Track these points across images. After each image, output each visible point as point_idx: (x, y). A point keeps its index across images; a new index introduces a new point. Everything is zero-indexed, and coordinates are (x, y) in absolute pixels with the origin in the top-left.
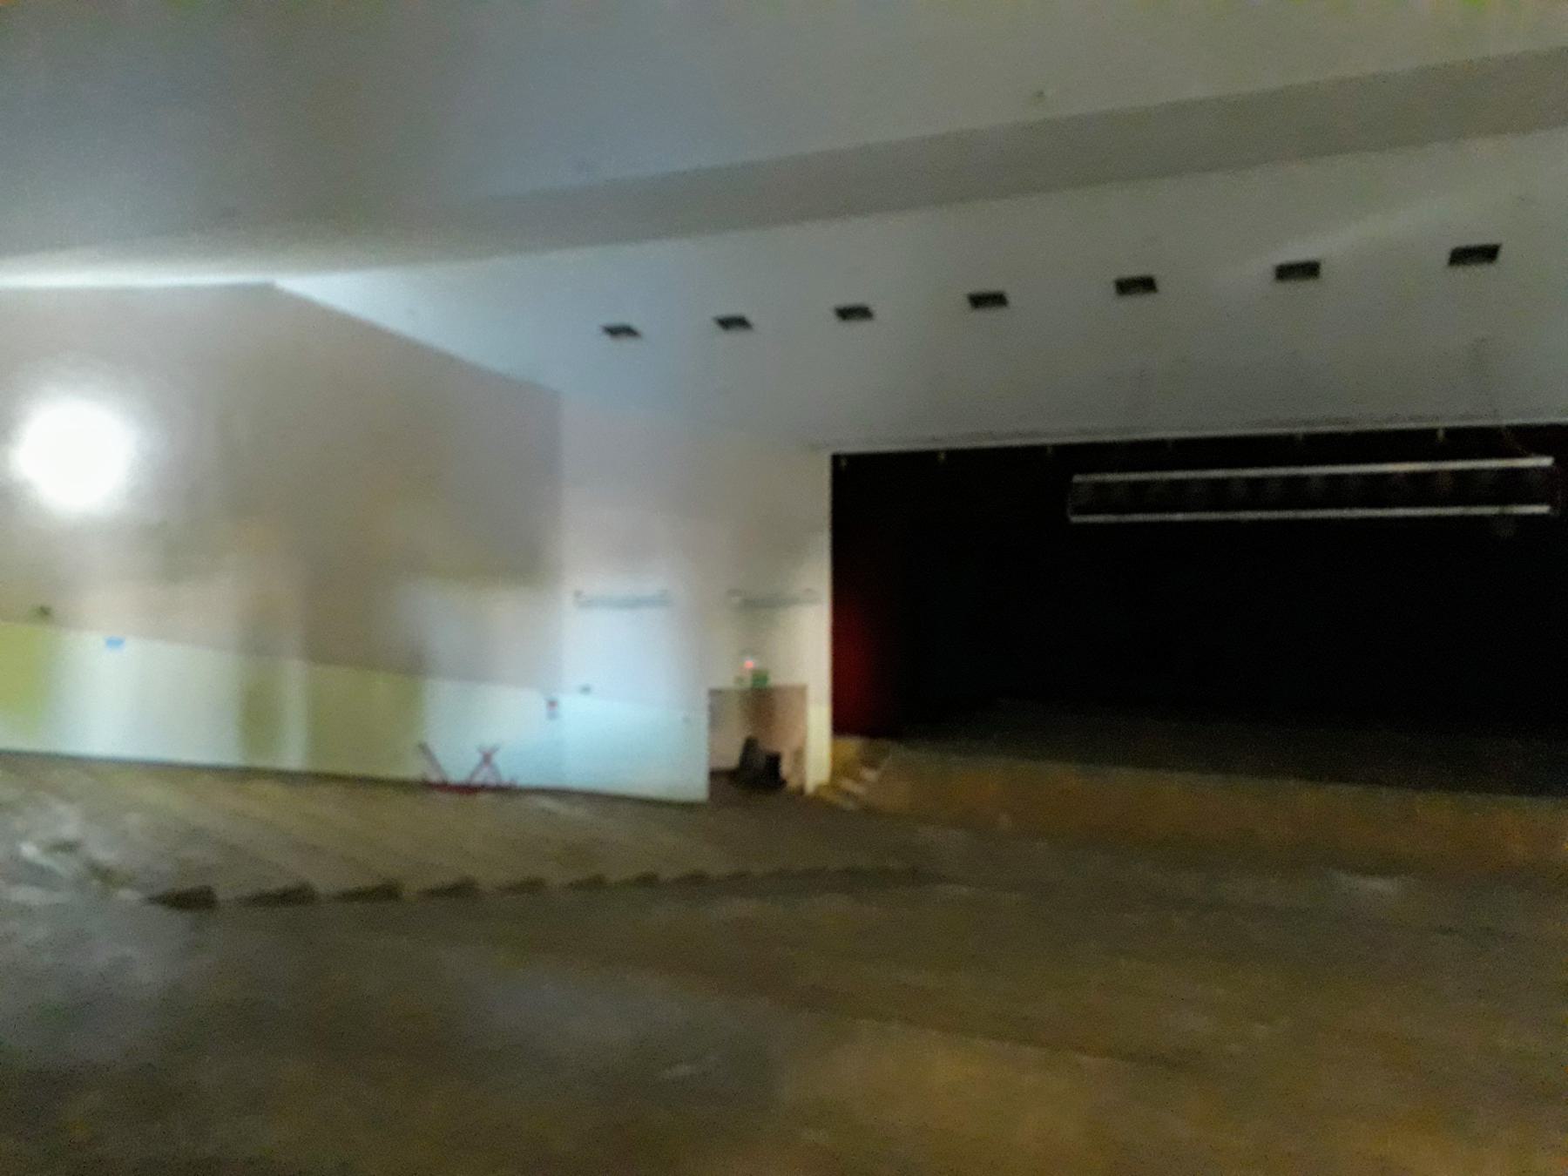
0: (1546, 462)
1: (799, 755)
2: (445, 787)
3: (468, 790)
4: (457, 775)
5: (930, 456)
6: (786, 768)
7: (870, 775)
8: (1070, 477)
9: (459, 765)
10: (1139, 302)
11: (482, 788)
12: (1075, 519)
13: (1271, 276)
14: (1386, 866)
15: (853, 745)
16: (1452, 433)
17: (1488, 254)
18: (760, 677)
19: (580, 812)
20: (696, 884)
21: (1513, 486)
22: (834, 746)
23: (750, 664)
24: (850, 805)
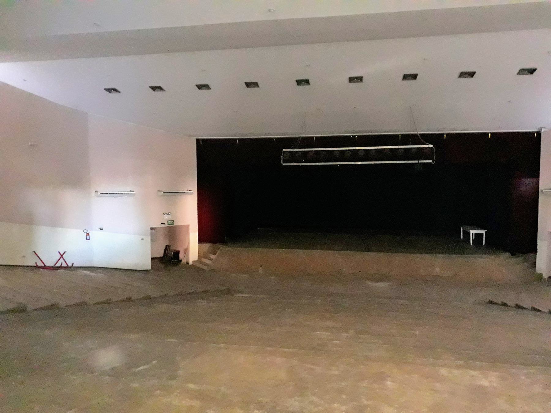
0: (431, 146)
1: (186, 251)
2: (45, 267)
3: (54, 268)
4: (49, 263)
5: (271, 140)
6: (181, 256)
7: (213, 257)
8: (282, 149)
9: (50, 260)
10: (303, 88)
11: (61, 267)
12: (284, 164)
13: (347, 80)
14: (384, 278)
15: (207, 246)
16: (360, 137)
17: (414, 77)
18: (171, 222)
19: (101, 276)
20: (148, 300)
21: (420, 155)
22: (199, 248)
23: (167, 217)
24: (205, 268)
